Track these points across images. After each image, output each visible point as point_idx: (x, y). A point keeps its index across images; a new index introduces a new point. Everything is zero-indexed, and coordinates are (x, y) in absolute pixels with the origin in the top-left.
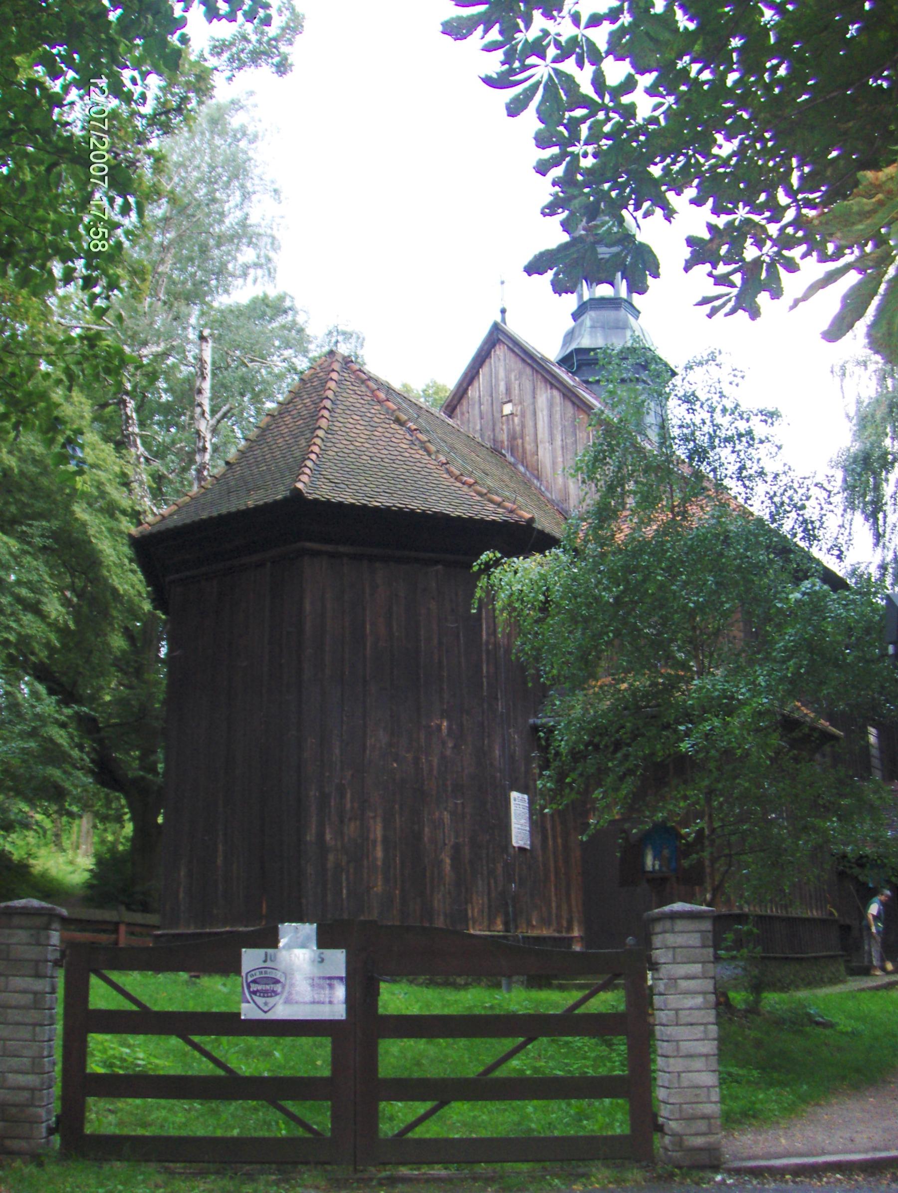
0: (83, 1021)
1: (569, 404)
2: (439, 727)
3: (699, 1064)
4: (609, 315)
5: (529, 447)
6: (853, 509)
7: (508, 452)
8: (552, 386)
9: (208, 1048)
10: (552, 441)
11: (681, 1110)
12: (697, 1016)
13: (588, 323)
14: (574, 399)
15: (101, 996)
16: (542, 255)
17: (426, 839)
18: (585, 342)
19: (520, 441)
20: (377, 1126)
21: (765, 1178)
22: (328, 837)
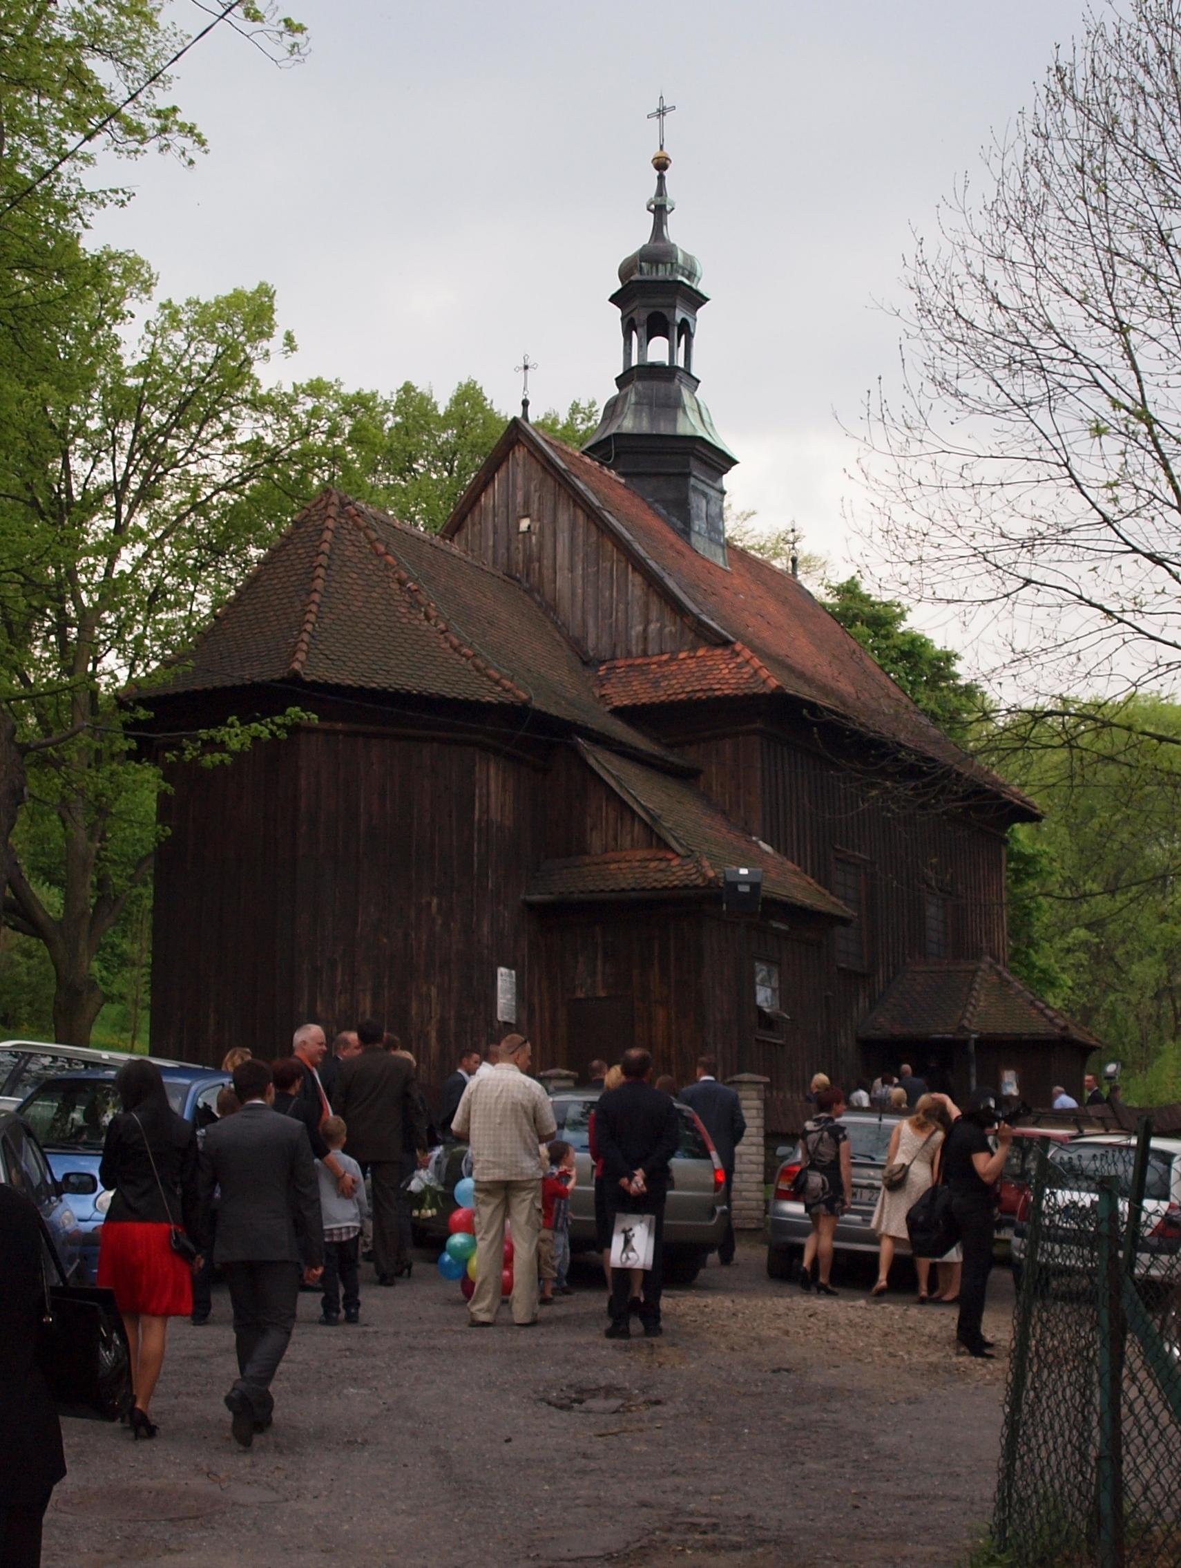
1: (593, 528)
2: (429, 904)
4: (659, 387)
8: (576, 504)
10: (572, 569)
14: (598, 523)
17: (413, 1012)
19: (537, 565)
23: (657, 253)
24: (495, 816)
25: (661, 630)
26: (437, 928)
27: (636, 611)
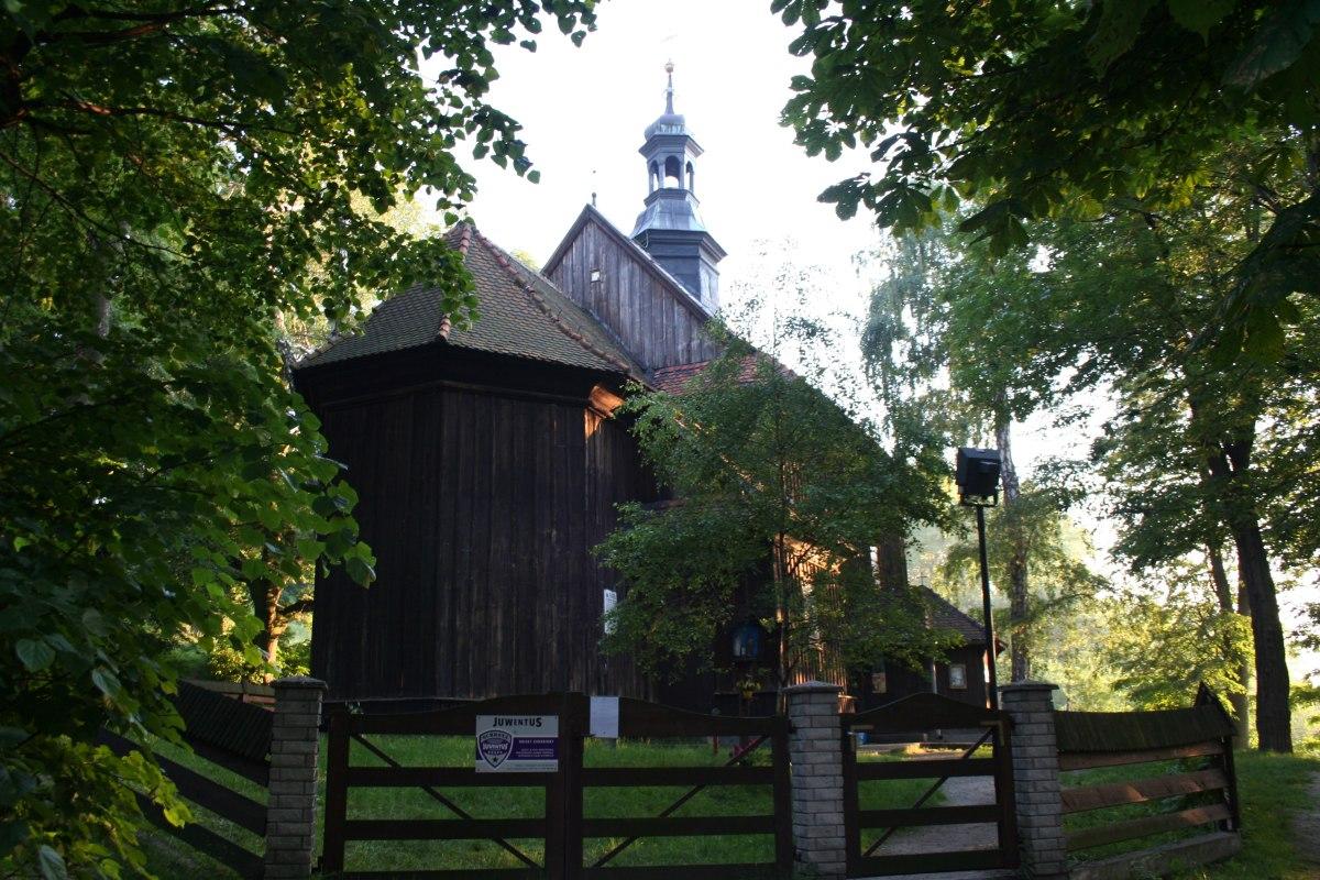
0: (343, 778)
1: (647, 276)
3: (829, 807)
4: (675, 203)
5: (613, 309)
6: (657, 172)
7: (597, 311)
8: (633, 260)
9: (657, 790)
11: (816, 843)
12: (829, 794)
13: (658, 209)
15: (358, 756)
16: (639, 218)
18: (656, 224)
20: (791, 829)
21: (998, 230)
22: (458, 623)
23: (670, 120)
24: (600, 466)
25: (701, 345)
26: (557, 555)
27: (681, 332)
